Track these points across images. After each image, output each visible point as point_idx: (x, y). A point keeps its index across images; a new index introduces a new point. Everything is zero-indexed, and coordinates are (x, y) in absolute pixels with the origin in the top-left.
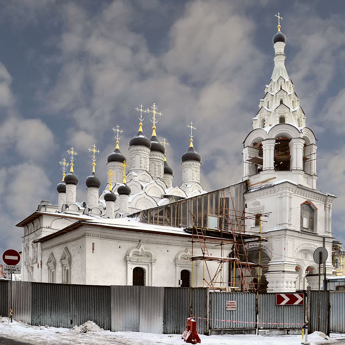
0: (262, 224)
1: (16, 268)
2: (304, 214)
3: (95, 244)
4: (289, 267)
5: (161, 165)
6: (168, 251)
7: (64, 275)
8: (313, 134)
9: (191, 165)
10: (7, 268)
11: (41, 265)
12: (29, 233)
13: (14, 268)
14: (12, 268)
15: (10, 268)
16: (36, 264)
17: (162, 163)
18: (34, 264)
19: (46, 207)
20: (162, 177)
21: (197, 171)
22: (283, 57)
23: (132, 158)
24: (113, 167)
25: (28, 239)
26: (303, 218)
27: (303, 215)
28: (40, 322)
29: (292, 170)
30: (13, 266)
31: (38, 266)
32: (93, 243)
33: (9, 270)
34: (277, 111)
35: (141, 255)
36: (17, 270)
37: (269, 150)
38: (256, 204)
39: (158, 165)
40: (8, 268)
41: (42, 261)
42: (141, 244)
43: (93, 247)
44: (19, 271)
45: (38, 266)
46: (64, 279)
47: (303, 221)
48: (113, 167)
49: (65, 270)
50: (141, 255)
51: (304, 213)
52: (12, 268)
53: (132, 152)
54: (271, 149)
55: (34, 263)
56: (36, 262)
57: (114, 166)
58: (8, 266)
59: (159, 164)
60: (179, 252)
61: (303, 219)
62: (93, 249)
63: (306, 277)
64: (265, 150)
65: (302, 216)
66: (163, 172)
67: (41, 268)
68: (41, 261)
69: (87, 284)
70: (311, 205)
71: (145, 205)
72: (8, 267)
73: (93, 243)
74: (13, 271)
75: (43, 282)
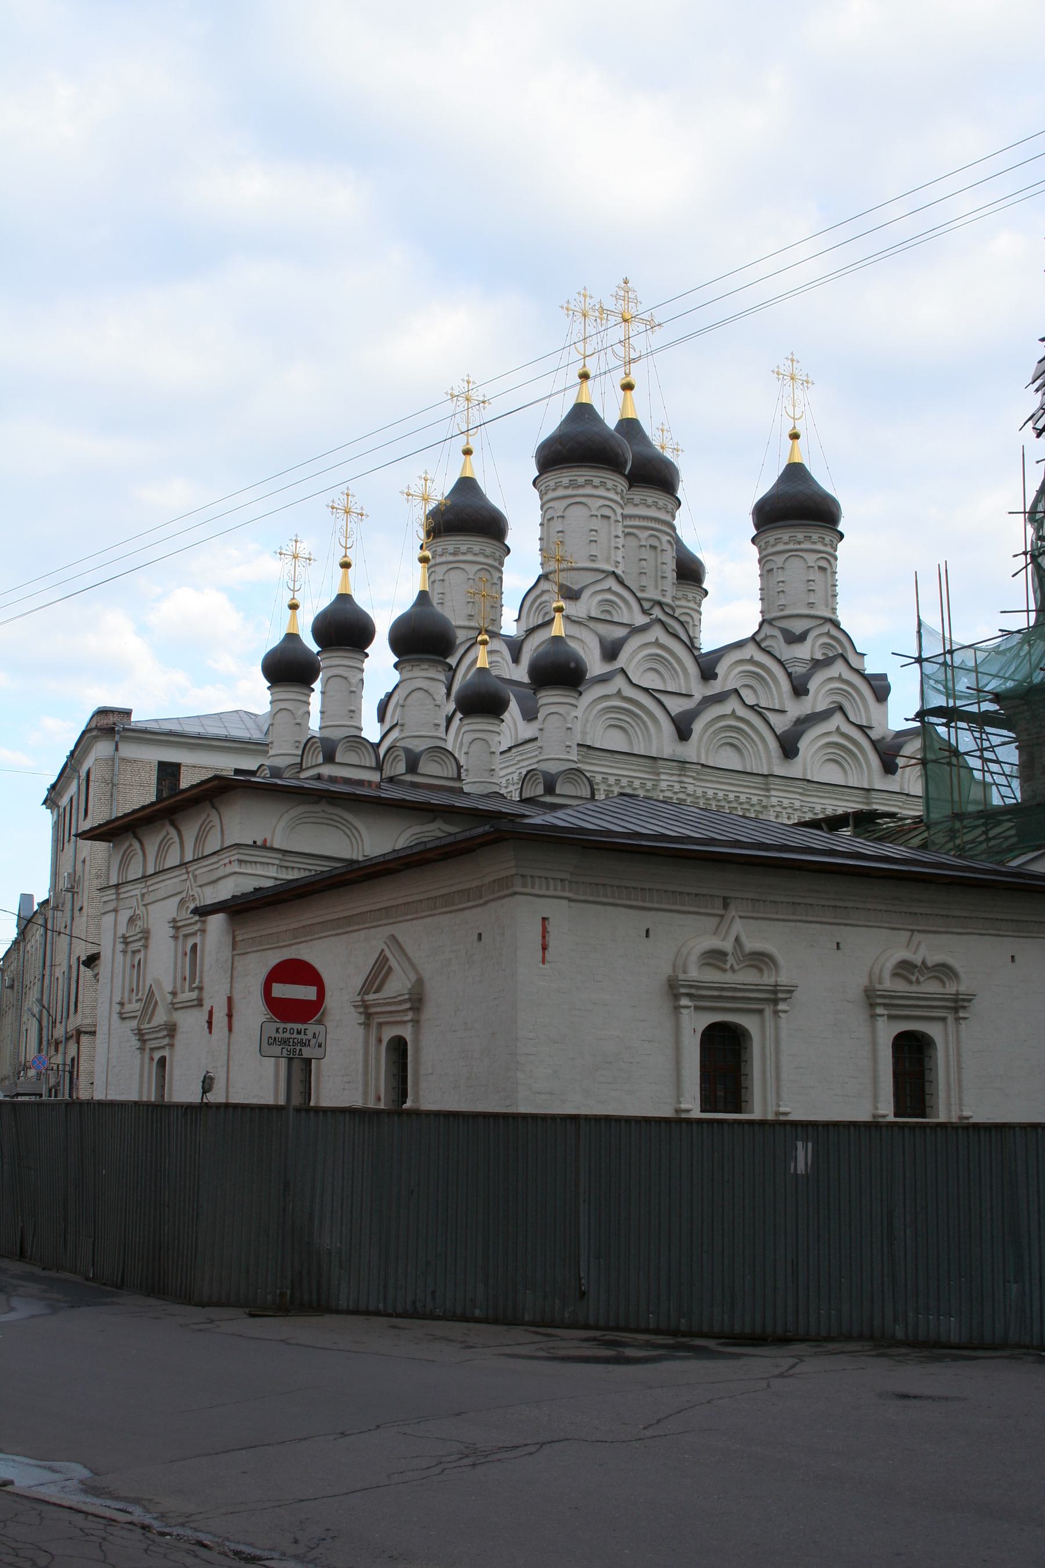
1: (310, 1036)
3: (551, 920)
5: (666, 546)
6: (841, 946)
7: (372, 1062)
9: (800, 543)
10: (277, 1035)
11: (230, 1016)
12: (150, 870)
13: (302, 1036)
14: (295, 1035)
15: (287, 1035)
16: (195, 1012)
17: (668, 538)
18: (176, 1009)
19: (117, 737)
20: (668, 600)
21: (608, 517)
23: (549, 520)
24: (451, 558)
25: (143, 895)
28: (433, 1293)
30: (299, 1026)
31: (210, 1023)
32: (544, 919)
33: (285, 1042)
35: (732, 966)
36: (313, 1041)
39: (651, 546)
40: (281, 1035)
41: (236, 997)
42: (733, 917)
43: (544, 937)
44: (320, 1046)
45: (210, 1023)
46: (372, 1083)
48: (451, 558)
49: (380, 1041)
50: (732, 966)
52: (295, 1035)
53: (770, 550)
55: (176, 1006)
56: (195, 1003)
57: (454, 554)
58: (282, 1026)
59: (655, 543)
62: (544, 948)
66: (672, 576)
67: (230, 1029)
68: (230, 1000)
69: (523, 1109)
71: (732, 745)
72: (281, 1031)
73: (544, 919)
74: (298, 1048)
75: (233, 1100)
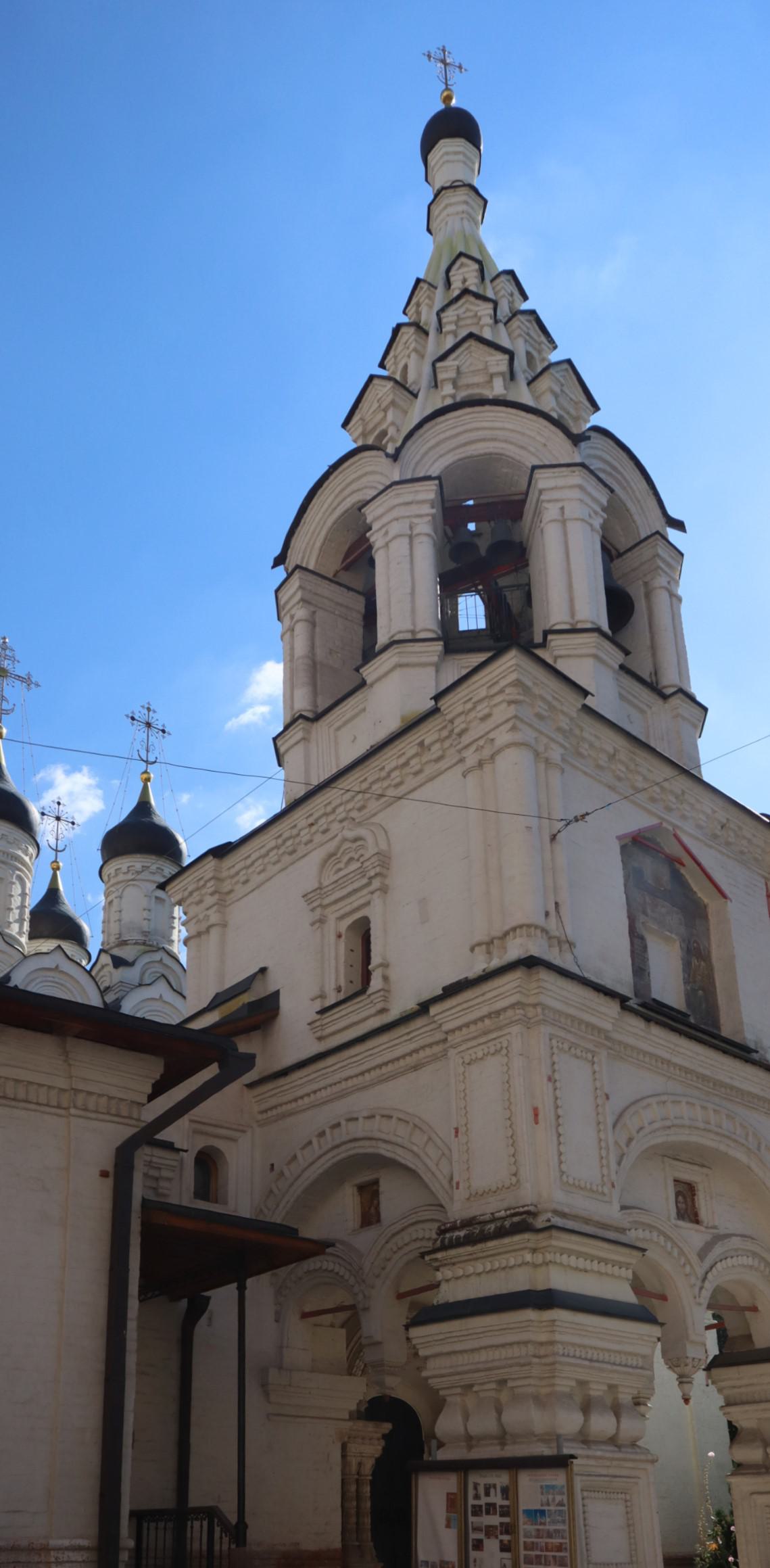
0: (408, 526)
2: (645, 913)
4: (581, 1263)
8: (651, 492)
22: (453, 200)
26: (642, 938)
27: (642, 918)
29: (546, 633)
34: (446, 369)
37: (406, 540)
38: (345, 859)
47: (645, 960)
51: (649, 911)
54: (419, 534)
60: (365, 1088)
61: (645, 947)
63: (715, 1371)
64: (387, 545)
65: (639, 926)
70: (683, 871)
